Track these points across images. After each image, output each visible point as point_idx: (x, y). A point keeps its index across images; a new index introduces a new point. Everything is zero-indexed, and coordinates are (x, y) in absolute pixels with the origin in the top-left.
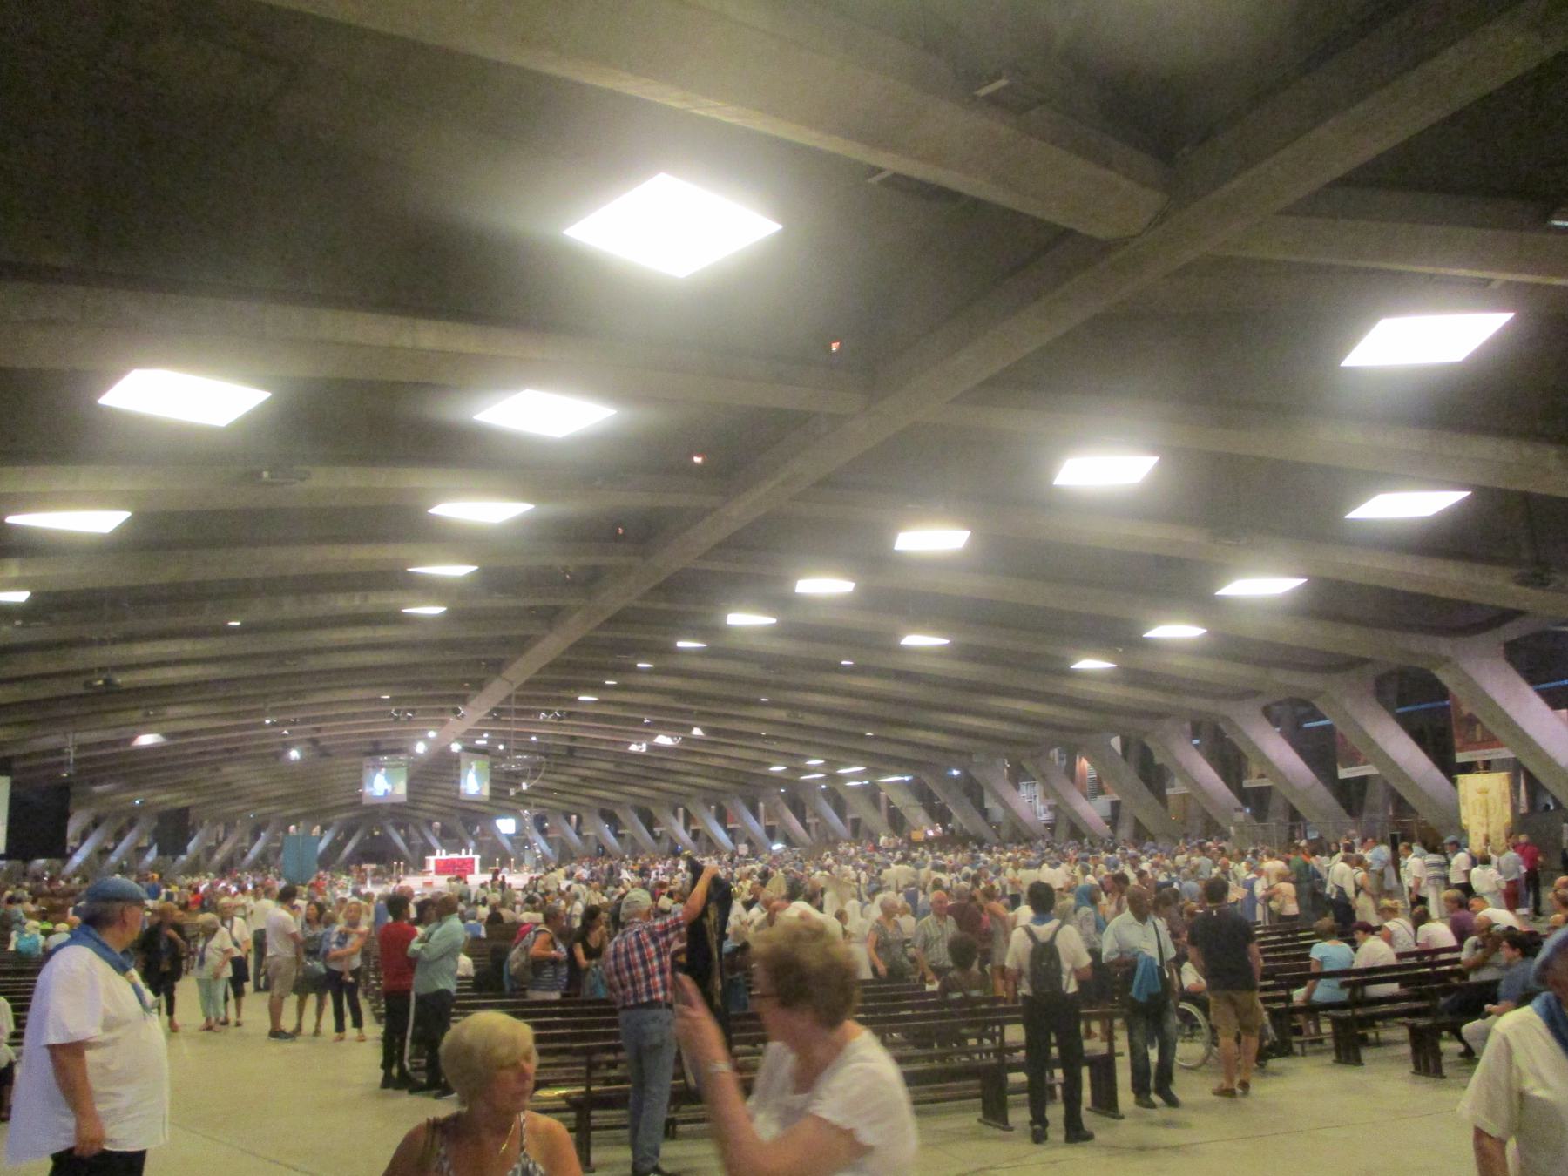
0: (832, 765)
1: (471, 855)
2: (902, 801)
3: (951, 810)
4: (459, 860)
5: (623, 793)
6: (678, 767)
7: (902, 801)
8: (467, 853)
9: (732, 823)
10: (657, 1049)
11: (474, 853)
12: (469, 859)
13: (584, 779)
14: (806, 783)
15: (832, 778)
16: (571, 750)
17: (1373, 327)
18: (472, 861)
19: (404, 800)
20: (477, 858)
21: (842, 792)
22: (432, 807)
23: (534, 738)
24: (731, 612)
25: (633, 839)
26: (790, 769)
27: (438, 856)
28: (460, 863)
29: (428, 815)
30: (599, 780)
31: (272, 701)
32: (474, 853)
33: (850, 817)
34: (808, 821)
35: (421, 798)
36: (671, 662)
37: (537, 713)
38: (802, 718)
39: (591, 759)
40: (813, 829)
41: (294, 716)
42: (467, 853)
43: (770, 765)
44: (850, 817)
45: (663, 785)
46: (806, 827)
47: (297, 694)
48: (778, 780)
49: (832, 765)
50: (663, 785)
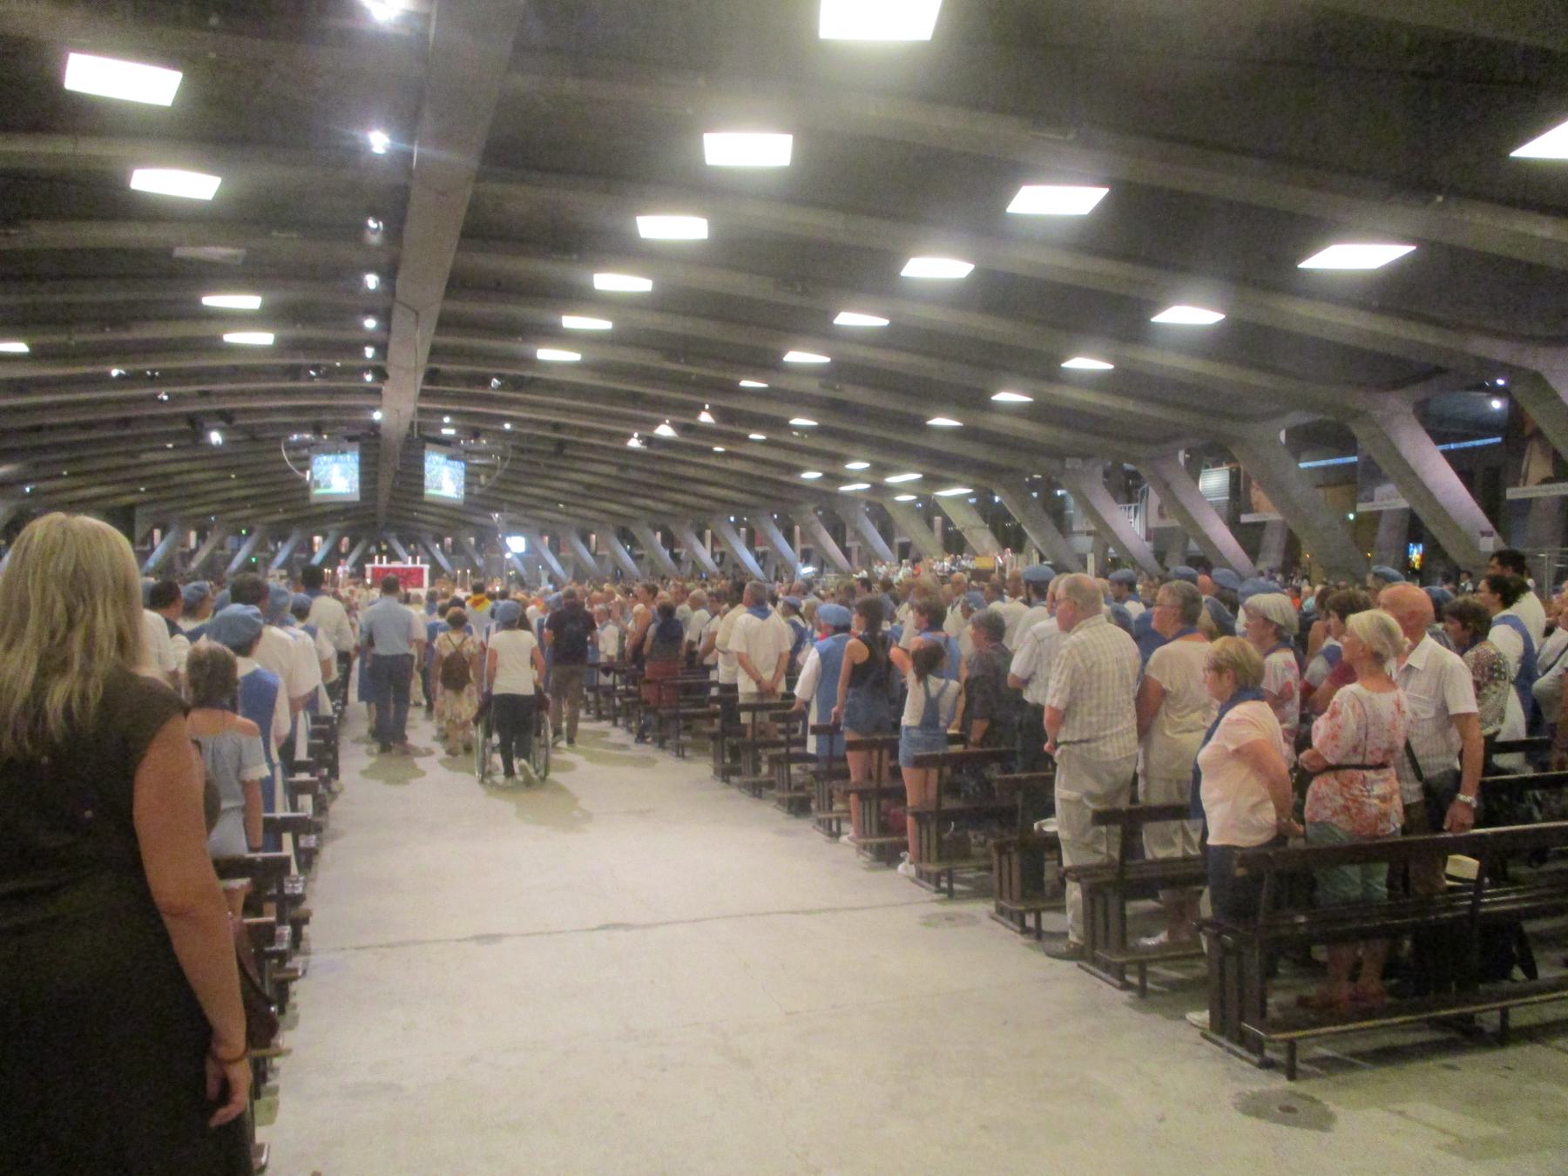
0: (880, 469)
1: (418, 565)
2: (965, 520)
3: (1026, 530)
4: (403, 569)
5: (635, 507)
6: (691, 472)
7: (965, 520)
8: (381, 561)
9: (761, 545)
10: (959, 661)
11: (422, 562)
12: (416, 569)
13: (589, 486)
14: (846, 497)
15: (879, 489)
16: (561, 444)
17: (1332, 271)
18: (421, 571)
19: (357, 498)
20: (426, 567)
21: (889, 508)
22: (431, 518)
23: (507, 426)
24: (704, 160)
25: (651, 562)
26: (828, 476)
27: (376, 564)
28: (405, 574)
29: (436, 529)
30: (607, 489)
31: (80, 331)
32: (422, 562)
33: (897, 540)
34: (848, 544)
35: (410, 506)
36: (784, 438)
37: (485, 381)
38: (840, 390)
39: (593, 461)
40: (855, 556)
41: (153, 366)
42: (414, 561)
43: (801, 469)
44: (897, 540)
45: (679, 497)
46: (846, 552)
47: (118, 317)
48: (810, 491)
49: (880, 469)
50: (679, 497)
